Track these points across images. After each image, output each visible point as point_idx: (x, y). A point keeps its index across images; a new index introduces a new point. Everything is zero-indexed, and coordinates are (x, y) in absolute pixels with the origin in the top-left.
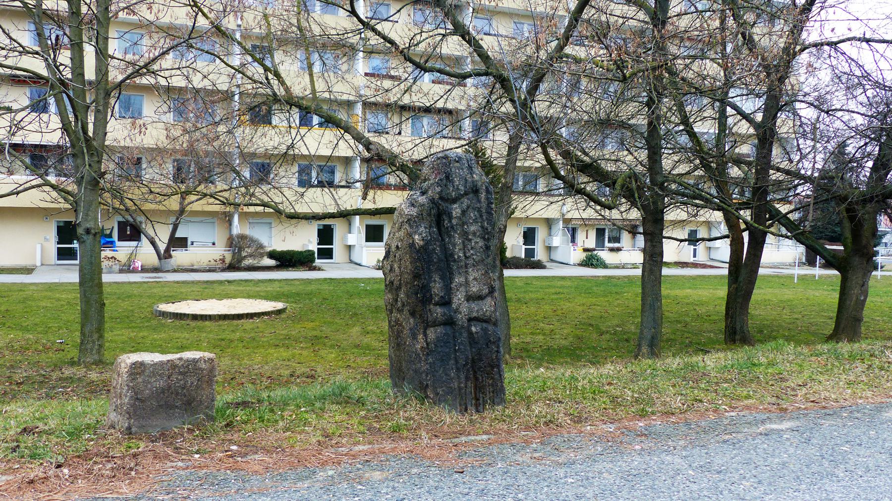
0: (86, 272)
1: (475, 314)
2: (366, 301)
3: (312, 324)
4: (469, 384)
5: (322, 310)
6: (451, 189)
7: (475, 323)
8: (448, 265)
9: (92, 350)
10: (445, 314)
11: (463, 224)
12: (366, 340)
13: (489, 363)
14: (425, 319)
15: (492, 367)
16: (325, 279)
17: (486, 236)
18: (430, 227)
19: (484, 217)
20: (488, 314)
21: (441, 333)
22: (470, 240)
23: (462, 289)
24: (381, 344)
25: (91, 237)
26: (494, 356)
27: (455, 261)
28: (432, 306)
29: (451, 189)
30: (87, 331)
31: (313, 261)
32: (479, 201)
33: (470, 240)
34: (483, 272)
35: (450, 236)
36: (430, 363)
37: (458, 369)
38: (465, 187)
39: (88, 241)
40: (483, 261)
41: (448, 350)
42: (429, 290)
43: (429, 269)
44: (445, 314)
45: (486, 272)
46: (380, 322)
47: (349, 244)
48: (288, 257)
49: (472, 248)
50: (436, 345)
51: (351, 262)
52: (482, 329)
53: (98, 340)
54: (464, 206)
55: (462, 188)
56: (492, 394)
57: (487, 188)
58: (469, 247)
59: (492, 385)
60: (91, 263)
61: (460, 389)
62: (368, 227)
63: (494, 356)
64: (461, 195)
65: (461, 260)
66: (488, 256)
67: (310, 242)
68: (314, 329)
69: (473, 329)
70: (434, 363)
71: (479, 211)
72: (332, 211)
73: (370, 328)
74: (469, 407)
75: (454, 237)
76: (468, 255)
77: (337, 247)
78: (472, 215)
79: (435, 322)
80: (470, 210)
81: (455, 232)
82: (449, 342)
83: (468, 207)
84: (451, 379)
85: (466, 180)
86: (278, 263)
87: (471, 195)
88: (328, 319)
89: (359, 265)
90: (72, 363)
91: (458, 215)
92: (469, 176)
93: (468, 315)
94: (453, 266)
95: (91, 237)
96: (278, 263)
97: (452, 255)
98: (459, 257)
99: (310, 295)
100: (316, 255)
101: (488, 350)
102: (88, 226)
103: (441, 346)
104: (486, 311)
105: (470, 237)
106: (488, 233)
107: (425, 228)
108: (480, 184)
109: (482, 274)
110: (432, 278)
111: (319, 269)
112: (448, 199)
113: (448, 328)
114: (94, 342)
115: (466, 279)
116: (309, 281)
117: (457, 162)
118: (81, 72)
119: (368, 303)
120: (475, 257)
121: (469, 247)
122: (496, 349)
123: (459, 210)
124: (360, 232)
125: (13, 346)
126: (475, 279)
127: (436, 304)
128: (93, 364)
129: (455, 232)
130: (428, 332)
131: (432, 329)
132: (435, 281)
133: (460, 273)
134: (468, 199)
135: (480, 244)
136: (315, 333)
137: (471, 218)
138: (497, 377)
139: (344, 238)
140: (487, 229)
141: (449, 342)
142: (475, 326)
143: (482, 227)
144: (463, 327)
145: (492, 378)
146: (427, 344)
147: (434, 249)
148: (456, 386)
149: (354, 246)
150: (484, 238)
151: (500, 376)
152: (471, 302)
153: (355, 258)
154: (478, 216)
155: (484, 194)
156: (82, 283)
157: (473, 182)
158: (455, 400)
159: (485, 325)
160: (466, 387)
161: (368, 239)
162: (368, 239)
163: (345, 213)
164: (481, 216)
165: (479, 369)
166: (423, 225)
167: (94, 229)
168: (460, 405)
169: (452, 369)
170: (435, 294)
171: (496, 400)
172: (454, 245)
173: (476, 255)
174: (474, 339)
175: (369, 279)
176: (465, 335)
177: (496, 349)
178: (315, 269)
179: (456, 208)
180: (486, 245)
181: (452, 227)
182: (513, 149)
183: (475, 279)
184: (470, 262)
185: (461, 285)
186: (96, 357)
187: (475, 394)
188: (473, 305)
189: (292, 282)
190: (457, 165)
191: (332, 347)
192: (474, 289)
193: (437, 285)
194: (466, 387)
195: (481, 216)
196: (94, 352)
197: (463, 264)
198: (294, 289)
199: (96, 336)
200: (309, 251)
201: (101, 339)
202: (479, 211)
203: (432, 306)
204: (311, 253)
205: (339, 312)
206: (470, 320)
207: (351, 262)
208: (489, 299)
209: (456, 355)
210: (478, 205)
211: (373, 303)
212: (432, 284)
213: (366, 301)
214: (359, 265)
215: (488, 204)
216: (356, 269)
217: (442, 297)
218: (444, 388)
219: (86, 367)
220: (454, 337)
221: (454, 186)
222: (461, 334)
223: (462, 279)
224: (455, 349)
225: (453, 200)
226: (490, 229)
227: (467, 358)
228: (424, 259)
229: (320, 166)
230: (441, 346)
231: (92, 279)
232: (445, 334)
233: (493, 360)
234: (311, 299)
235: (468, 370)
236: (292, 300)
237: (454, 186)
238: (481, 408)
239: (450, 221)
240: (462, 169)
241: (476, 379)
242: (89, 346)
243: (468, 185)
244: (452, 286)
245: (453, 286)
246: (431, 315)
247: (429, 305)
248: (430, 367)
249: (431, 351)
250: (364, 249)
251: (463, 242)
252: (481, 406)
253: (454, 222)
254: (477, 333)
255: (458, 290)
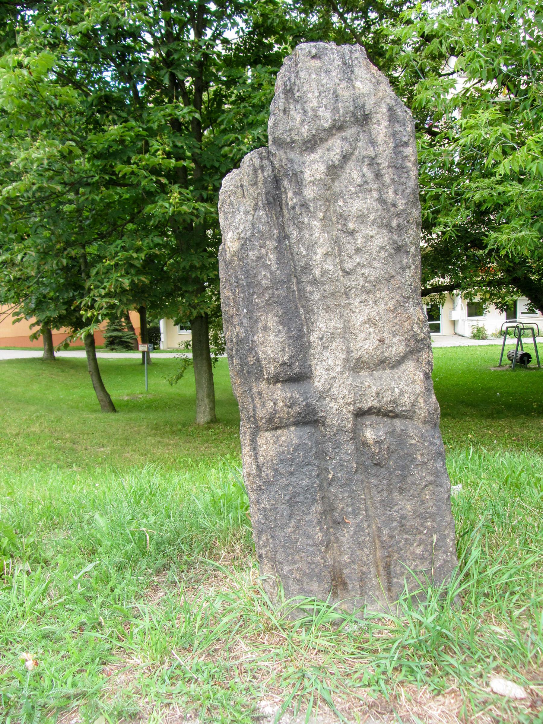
14: (251, 413)
17: (394, 223)
18: (256, 208)
19: (387, 179)
21: (289, 444)
22: (352, 233)
23: (338, 344)
27: (314, 282)
28: (263, 385)
29: (299, 117)
35: (300, 226)
38: (335, 110)
49: (358, 251)
50: (276, 471)
51: (456, 334)
54: (335, 157)
57: (390, 109)
69: (369, 435)
70: (274, 509)
71: (373, 162)
75: (310, 228)
76: (348, 266)
77: (444, 322)
78: (355, 174)
80: (351, 164)
85: (336, 97)
91: (318, 177)
94: (312, 293)
104: (402, 392)
105: (351, 226)
109: (389, 310)
113: (306, 431)
121: (351, 248)
124: (462, 309)
126: (370, 321)
127: (276, 379)
132: (266, 328)
134: (345, 139)
139: (449, 314)
140: (395, 205)
143: (382, 201)
146: (259, 467)
153: (459, 330)
154: (370, 175)
164: (378, 176)
172: (311, 246)
173: (370, 265)
176: (349, 448)
179: (313, 162)
181: (304, 205)
182: (510, 98)
183: (370, 321)
184: (358, 281)
185: (333, 337)
193: (272, 337)
195: (378, 176)
202: (373, 162)
206: (360, 414)
207: (456, 334)
208: (409, 366)
215: (396, 146)
217: (284, 364)
221: (305, 112)
223: (335, 323)
237: (305, 112)
239: (299, 192)
240: (327, 72)
244: (312, 339)
248: (266, 517)
249: (269, 483)
253: (309, 192)
254: (379, 443)
255: (325, 348)
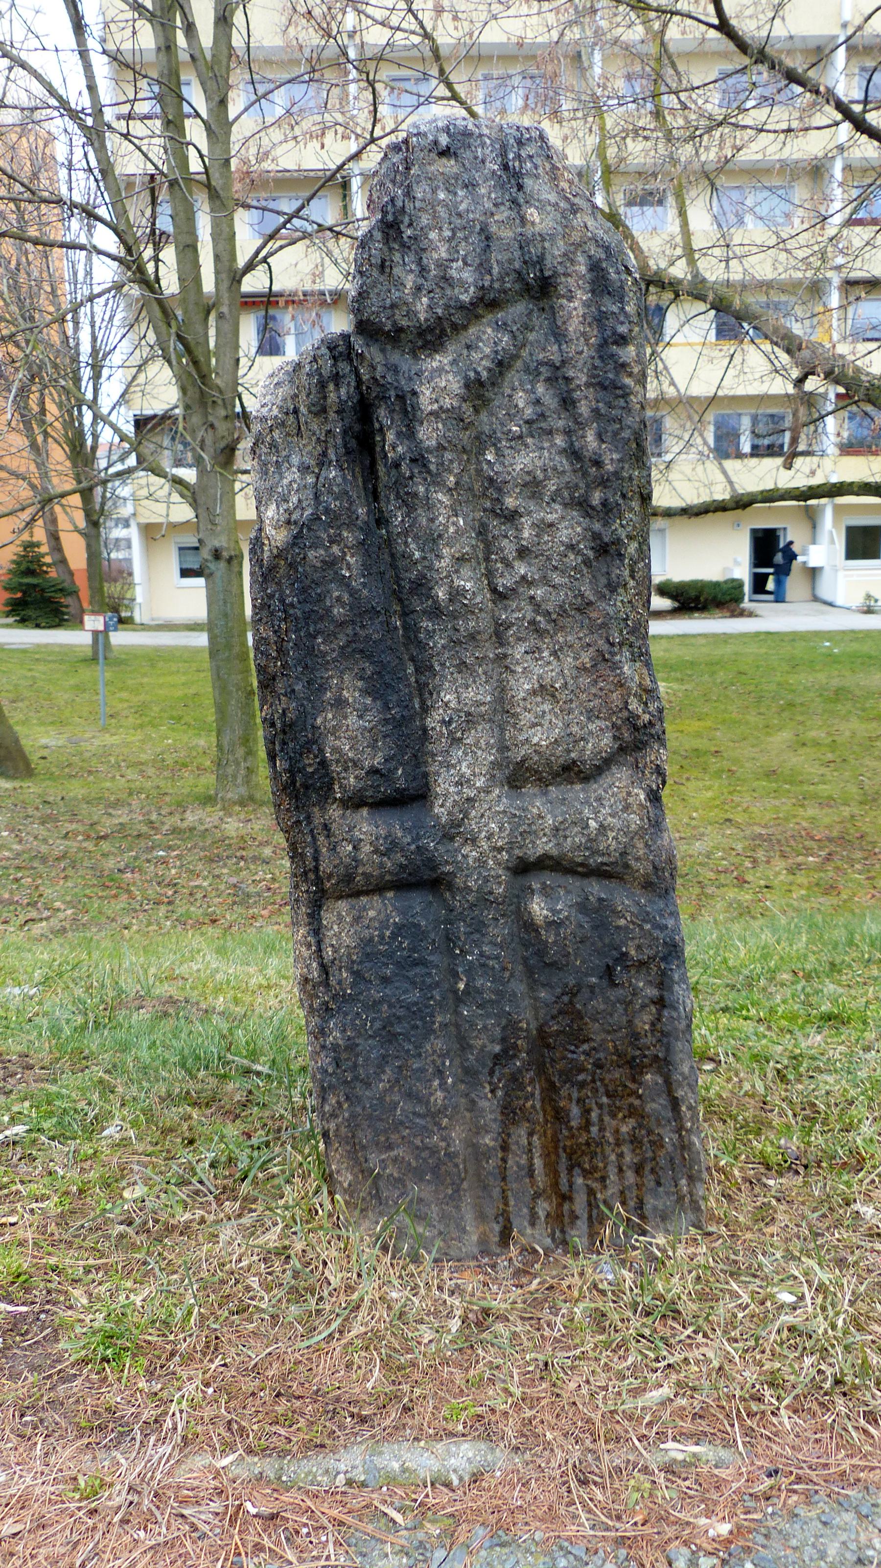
0: (217, 631)
1: (543, 846)
2: (821, 677)
3: (697, 723)
4: (520, 1134)
5: (727, 696)
6: (410, 281)
7: (549, 879)
8: (412, 631)
9: (235, 777)
10: (393, 845)
11: (482, 442)
12: (798, 760)
13: (617, 1052)
15: (635, 1068)
16: (757, 634)
17: (596, 497)
18: (322, 461)
19: (584, 409)
20: (610, 842)
21: (384, 925)
22: (512, 517)
24: (823, 770)
25: (222, 565)
26: (644, 1022)
27: (436, 612)
28: (334, 812)
29: (410, 281)
30: (225, 742)
31: (739, 599)
32: (558, 335)
33: (512, 517)
34: (586, 658)
35: (409, 502)
36: (335, 1047)
37: (469, 1074)
38: (483, 267)
39: (218, 574)
40: (584, 607)
41: (415, 995)
42: (313, 744)
43: (311, 651)
44: (393, 845)
45: (602, 658)
46: (836, 721)
47: (812, 564)
48: (693, 594)
49: (523, 553)
50: (357, 974)
51: (816, 599)
52: (583, 907)
53: (245, 760)
55: (468, 275)
56: (630, 1177)
58: (509, 548)
59: (635, 1141)
60: (226, 615)
61: (478, 1154)
62: (852, 532)
63: (644, 1022)
64: (462, 307)
65: (469, 610)
66: (612, 588)
67: (737, 563)
68: (698, 735)
69: (538, 908)
70: (351, 1047)
72: (719, 497)
73: (812, 734)
74: (520, 1223)
75: (429, 505)
76: (504, 582)
78: (521, 399)
79: (348, 878)
80: (514, 377)
81: (436, 481)
82: (422, 962)
83: (502, 365)
84: (434, 1115)
86: (676, 605)
87: (518, 310)
88: (734, 715)
89: (831, 604)
90: (208, 800)
92: (503, 214)
93: (510, 846)
94: (430, 634)
95: (222, 565)
96: (676, 605)
97: (422, 586)
98: (456, 594)
99: (713, 665)
100: (747, 588)
101: (613, 994)
102: (217, 544)
103: (385, 980)
104: (603, 828)
105: (510, 502)
106: (603, 483)
107: (304, 469)
108: (557, 250)
109: (582, 669)
110: (322, 689)
111: (751, 614)
112: (400, 330)
113: (417, 901)
114: (238, 764)
115: (502, 689)
116: (725, 638)
117: (445, 153)
118: (189, 242)
119: (824, 681)
120: (539, 592)
121: (509, 548)
122: (652, 992)
123: (453, 383)
124: (832, 542)
125: (163, 760)
126: (544, 690)
128: (235, 803)
129: (436, 481)
130: (328, 917)
131: (343, 906)
132: (340, 703)
133: (462, 666)
134: (503, 327)
135: (564, 534)
136: (698, 743)
137: (513, 413)
138: (656, 1106)
140: (598, 463)
141: (422, 962)
142: (547, 892)
143: (574, 454)
144: (485, 899)
145: (632, 1112)
146: (324, 968)
147: (331, 564)
148: (457, 1145)
149: (820, 569)
150: (583, 505)
151: (675, 1104)
152: (529, 789)
154: (550, 401)
155: (582, 296)
156: (214, 650)
157: (523, 244)
158: (455, 1197)
159: (596, 889)
160: (505, 1148)
161: (851, 554)
162: (851, 554)
163: (745, 499)
164: (567, 403)
165: (567, 1076)
166: (295, 460)
167: (228, 549)
168: (481, 1217)
169: (440, 1073)
170: (348, 764)
171: (650, 1202)
172: (432, 540)
173: (545, 580)
174: (541, 953)
175: (843, 632)
176: (499, 931)
177: (652, 992)
178: (742, 614)
179: (440, 370)
180: (596, 536)
181: (419, 460)
183: (544, 690)
185: (471, 720)
186: (243, 790)
187: (552, 1169)
188: (538, 805)
189: (693, 641)
190: (449, 166)
191: (718, 774)
192: (538, 737)
193: (352, 720)
194: (505, 1148)
195: (567, 403)
196: (239, 781)
197: (482, 623)
198: (687, 654)
199: (240, 752)
200: (733, 580)
201: (250, 758)
203: (334, 812)
204: (737, 585)
205: (759, 699)
209: (457, 1013)
210: (553, 352)
211: (835, 682)
212: (326, 718)
213: (821, 677)
214: (831, 604)
215: (604, 344)
216: (823, 613)
218: (399, 1152)
219: (224, 809)
220: (449, 939)
221: (423, 270)
222: (479, 927)
224: (455, 991)
225: (421, 333)
226: (611, 459)
227: (511, 1027)
228: (286, 608)
229: (772, 416)
230: (385, 980)
231: (229, 646)
232: (399, 930)
233: (636, 1036)
234: (713, 674)
235: (514, 1078)
236: (679, 675)
237: (423, 270)
238: (578, 1238)
239: (409, 433)
241: (559, 1116)
242: (230, 770)
243: (496, 255)
245: (433, 721)
246: (333, 849)
247: (323, 809)
250: (841, 574)
251: (482, 531)
252: (582, 1225)
255: (456, 741)
